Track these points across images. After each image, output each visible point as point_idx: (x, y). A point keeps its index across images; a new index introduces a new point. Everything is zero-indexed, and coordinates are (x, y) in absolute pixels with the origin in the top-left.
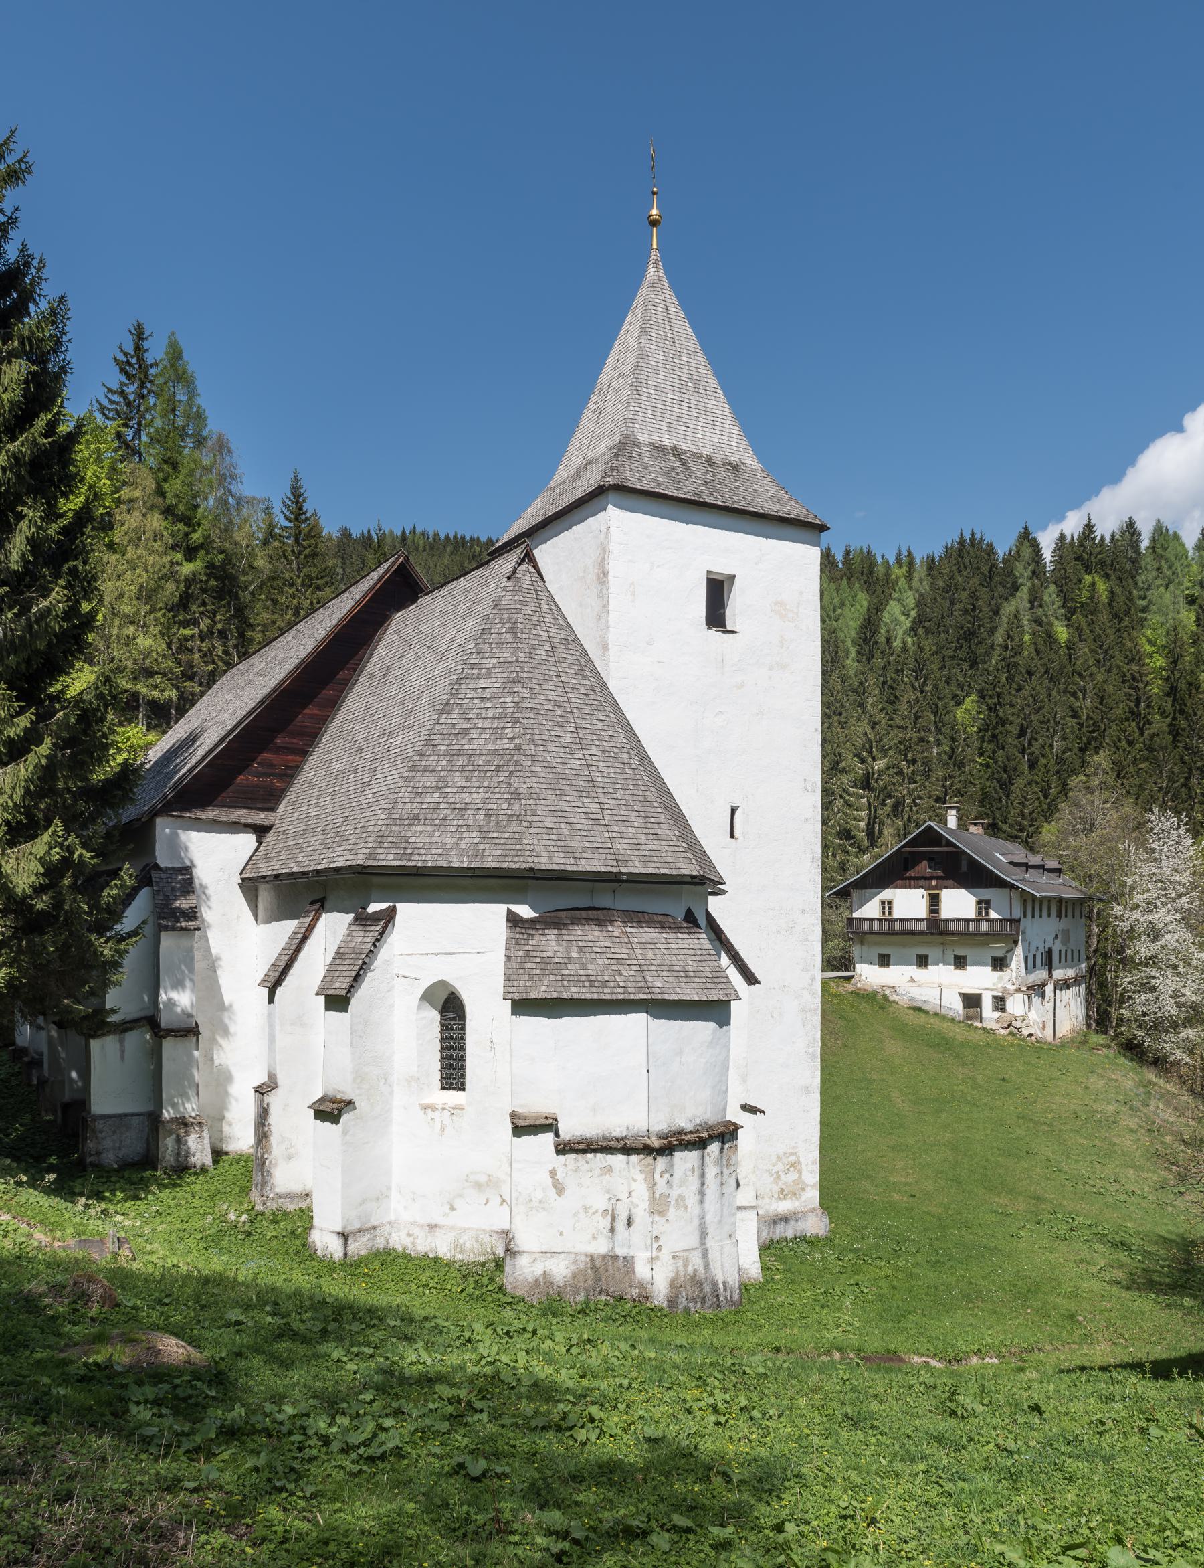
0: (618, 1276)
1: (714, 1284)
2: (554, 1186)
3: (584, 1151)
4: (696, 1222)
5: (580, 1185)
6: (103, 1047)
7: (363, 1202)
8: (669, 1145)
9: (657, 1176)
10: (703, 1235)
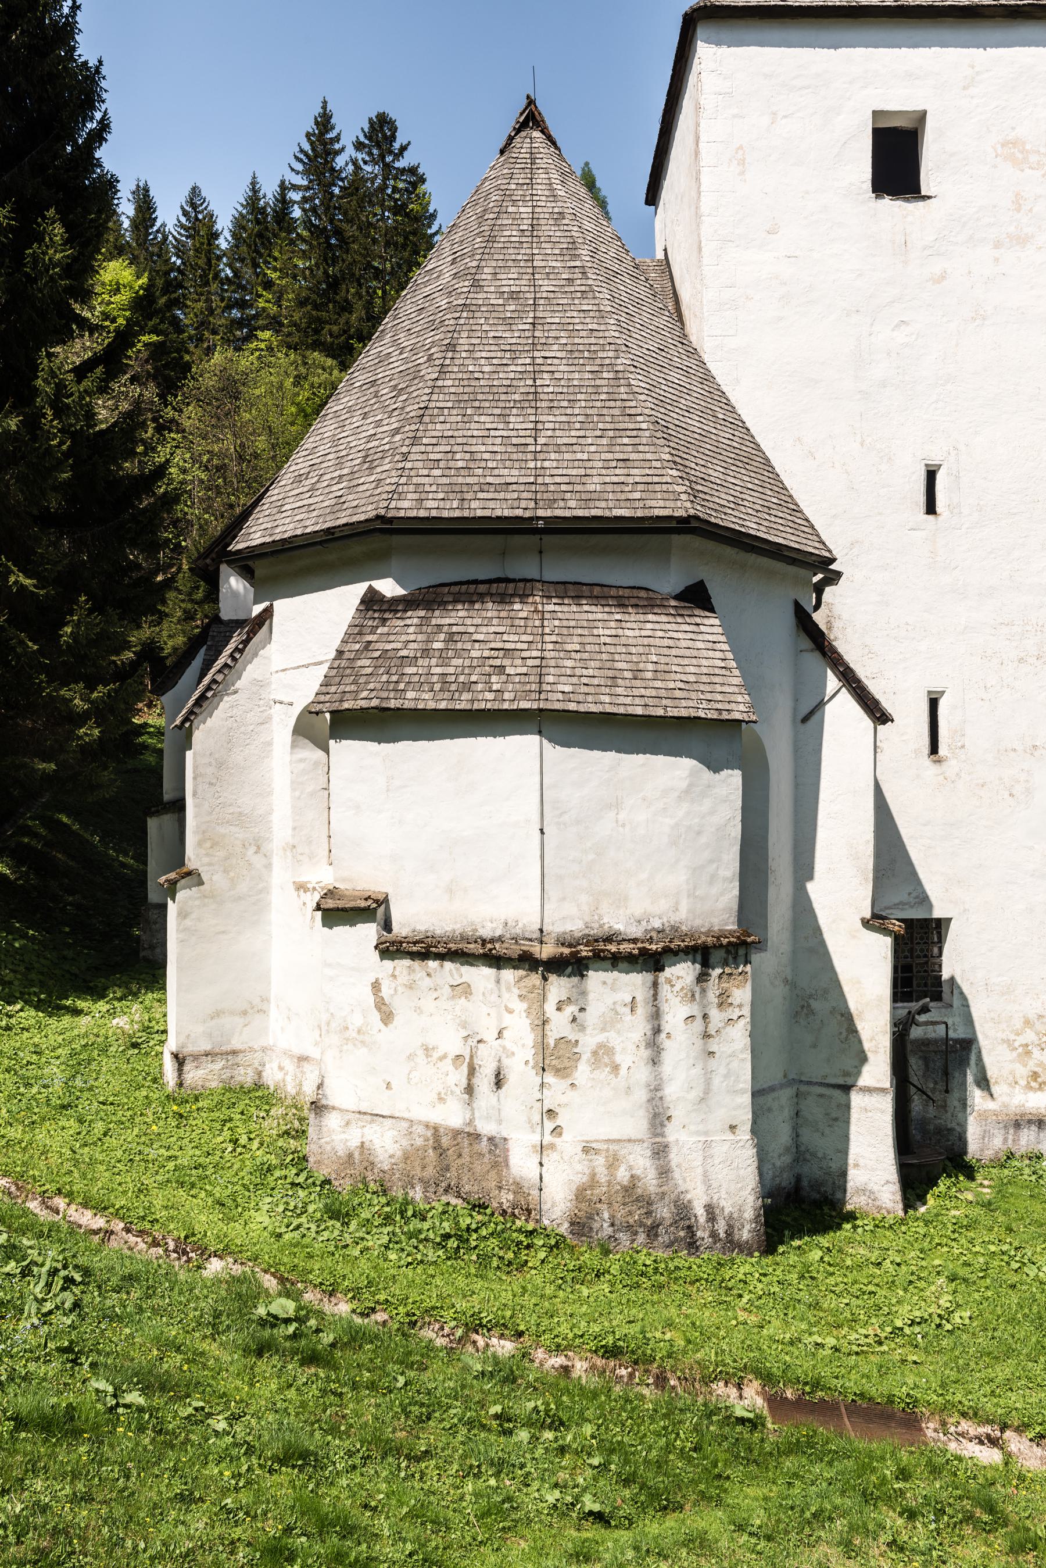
0: (478, 1168)
1: (683, 1211)
2: (379, 1009)
3: (424, 955)
4: (641, 1095)
5: (418, 1010)
6: (160, 827)
7: (217, 1014)
8: (575, 960)
9: (550, 1007)
10: (658, 1118)
